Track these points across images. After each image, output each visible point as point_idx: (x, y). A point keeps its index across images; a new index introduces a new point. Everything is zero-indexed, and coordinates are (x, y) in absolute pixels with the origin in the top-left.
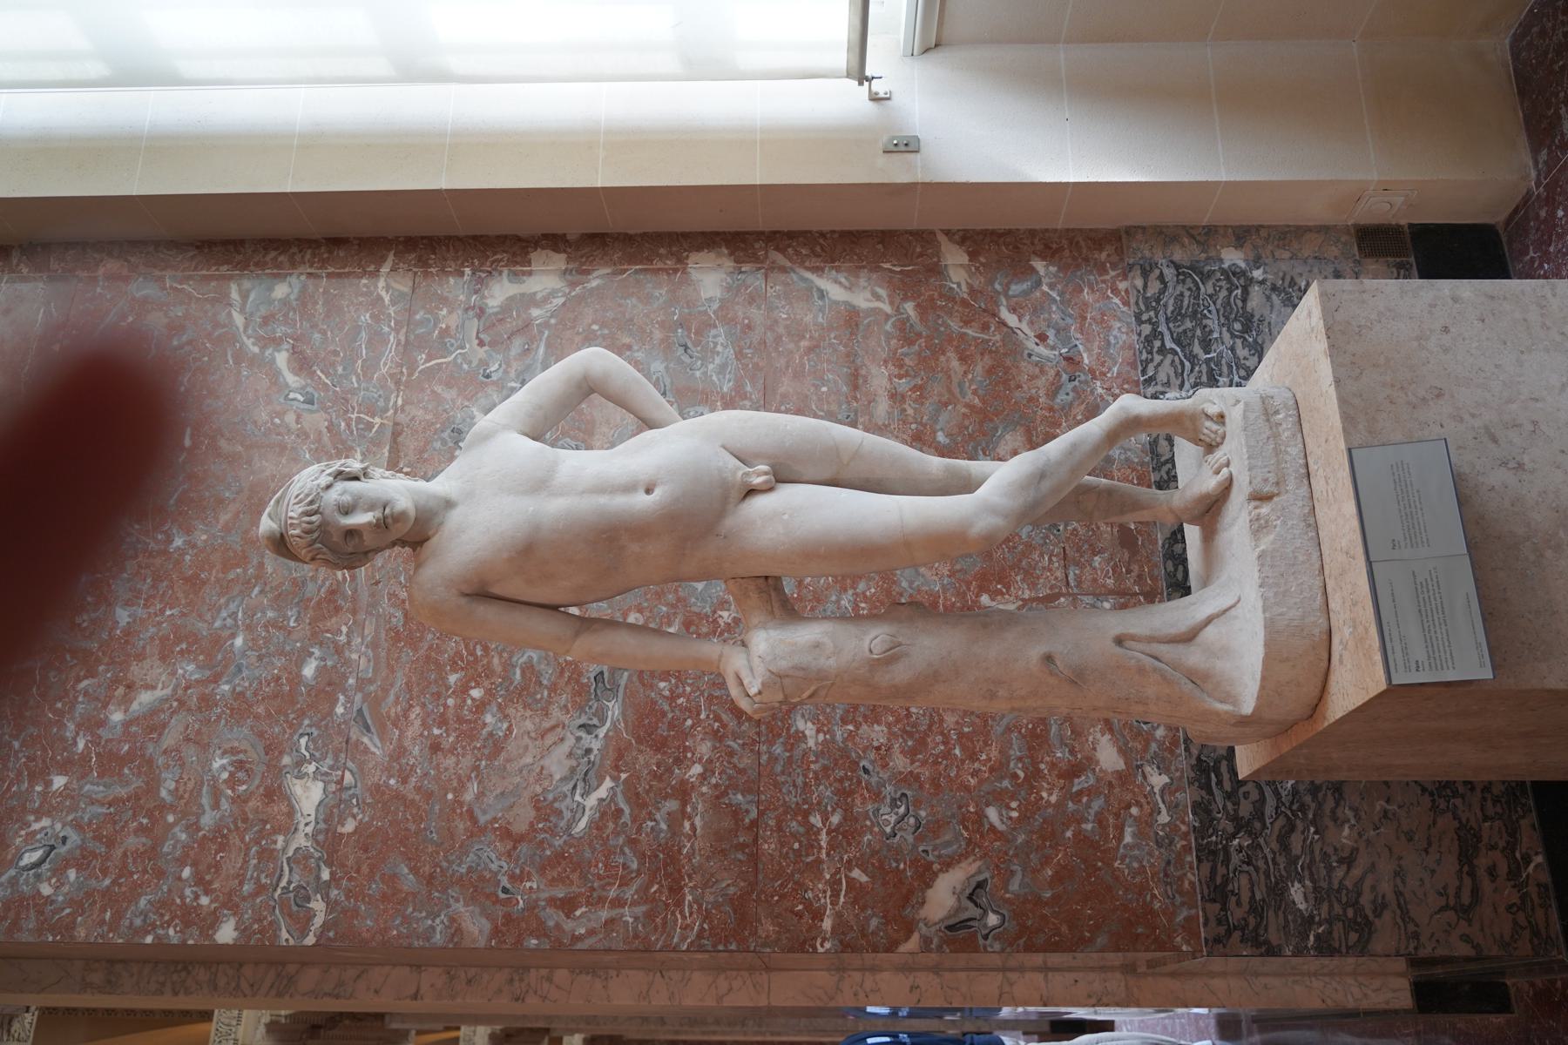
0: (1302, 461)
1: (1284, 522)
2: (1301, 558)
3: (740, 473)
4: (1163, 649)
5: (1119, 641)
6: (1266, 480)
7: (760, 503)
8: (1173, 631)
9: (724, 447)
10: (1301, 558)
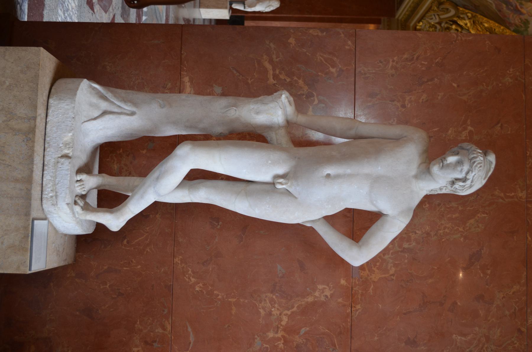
0: (45, 172)
2: (54, 128)
3: (289, 184)
4: (116, 110)
5: (133, 114)
6: (62, 164)
7: (281, 170)
8: (111, 116)
9: (296, 198)
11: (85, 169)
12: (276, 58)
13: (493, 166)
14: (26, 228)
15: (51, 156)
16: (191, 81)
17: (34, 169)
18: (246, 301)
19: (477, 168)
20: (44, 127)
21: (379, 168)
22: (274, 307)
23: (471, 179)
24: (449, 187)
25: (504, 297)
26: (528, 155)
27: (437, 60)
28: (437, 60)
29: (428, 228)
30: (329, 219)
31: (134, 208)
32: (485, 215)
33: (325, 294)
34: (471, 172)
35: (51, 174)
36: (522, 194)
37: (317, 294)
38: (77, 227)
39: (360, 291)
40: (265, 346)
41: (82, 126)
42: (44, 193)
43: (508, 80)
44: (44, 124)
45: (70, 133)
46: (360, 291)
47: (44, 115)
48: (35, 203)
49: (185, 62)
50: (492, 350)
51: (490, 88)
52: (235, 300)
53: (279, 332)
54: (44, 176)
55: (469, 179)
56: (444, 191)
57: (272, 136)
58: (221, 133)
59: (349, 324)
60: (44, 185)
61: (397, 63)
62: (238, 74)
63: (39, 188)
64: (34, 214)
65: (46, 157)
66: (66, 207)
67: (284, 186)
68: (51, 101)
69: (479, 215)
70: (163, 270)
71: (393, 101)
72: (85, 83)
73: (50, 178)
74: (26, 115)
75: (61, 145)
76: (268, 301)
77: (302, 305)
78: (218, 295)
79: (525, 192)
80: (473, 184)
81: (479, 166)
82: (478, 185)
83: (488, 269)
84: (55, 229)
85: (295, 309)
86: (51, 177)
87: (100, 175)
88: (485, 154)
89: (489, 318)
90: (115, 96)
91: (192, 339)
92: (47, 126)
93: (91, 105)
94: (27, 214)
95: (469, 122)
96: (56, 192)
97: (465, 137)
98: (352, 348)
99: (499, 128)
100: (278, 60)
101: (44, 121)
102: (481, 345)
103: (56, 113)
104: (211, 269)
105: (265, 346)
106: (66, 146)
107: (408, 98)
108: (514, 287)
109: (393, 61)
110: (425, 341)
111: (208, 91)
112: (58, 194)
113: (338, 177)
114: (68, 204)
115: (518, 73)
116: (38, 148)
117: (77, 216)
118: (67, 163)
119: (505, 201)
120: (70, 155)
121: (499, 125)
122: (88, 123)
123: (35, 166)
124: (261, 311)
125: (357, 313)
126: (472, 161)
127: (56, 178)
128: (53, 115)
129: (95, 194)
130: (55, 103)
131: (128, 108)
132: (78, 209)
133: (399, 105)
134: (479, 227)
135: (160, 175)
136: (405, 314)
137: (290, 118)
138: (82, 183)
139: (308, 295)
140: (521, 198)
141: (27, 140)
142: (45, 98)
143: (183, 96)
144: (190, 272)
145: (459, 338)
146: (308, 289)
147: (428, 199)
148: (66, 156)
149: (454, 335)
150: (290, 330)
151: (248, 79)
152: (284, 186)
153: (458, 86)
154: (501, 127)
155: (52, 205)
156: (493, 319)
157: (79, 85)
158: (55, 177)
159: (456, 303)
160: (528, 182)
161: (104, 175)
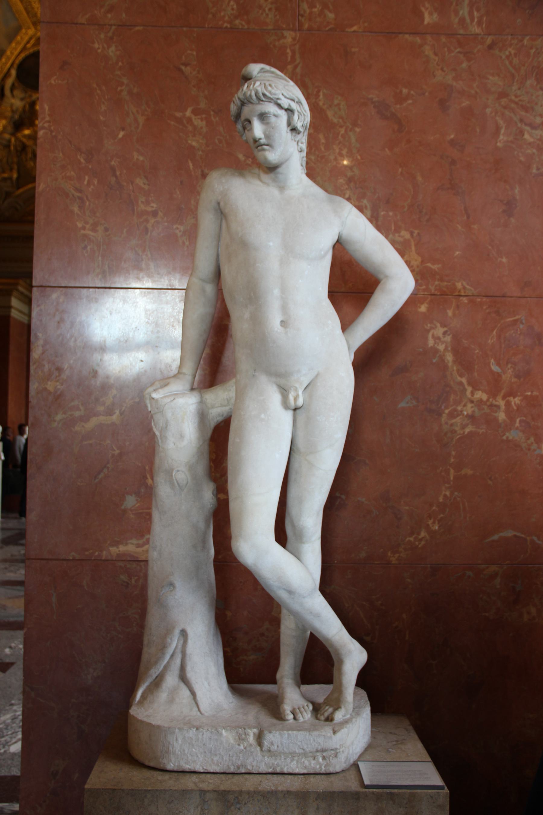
1: (241, 752)
2: (215, 759)
3: (297, 385)
4: (178, 661)
5: (184, 633)
6: (272, 744)
7: (275, 398)
8: (188, 668)
9: (317, 375)
10: (215, 759)
11: (273, 707)
12: (80, 410)
13: (267, 67)
14: (378, 798)
15: (260, 762)
16: (117, 544)
17: (285, 789)
18: (453, 453)
19: (273, 91)
20: (213, 776)
21: (271, 244)
22: (462, 411)
23: (290, 101)
24: (299, 137)
25: (442, 69)
26: (229, 26)
27: (82, 160)
28: (82, 160)
29: (341, 181)
30: (345, 326)
31: (330, 625)
32: (321, 94)
33: (441, 335)
34: (279, 101)
35: (288, 760)
36: (289, 37)
37: (441, 347)
38: (364, 715)
39: (437, 283)
40: (517, 424)
41: (206, 714)
42: (318, 771)
43: (112, 51)
44: (209, 776)
45: (221, 734)
46: (437, 283)
47: (194, 778)
48: (337, 785)
49: (87, 553)
50: (519, 89)
51: (125, 80)
52: (452, 471)
53: (497, 403)
54: (291, 771)
55: (290, 105)
56: (304, 146)
57: (216, 414)
58: (213, 494)
59: (484, 299)
60: (305, 771)
61: (87, 223)
62: (105, 470)
63: (312, 779)
64: (354, 786)
65: (261, 770)
66: (339, 735)
67: (300, 393)
68: (171, 766)
69: (321, 104)
70: (409, 580)
71: (146, 230)
72: (137, 712)
73: (295, 762)
74: (197, 807)
75: (242, 747)
76: (453, 421)
77: (458, 370)
78: (445, 496)
79: (286, 33)
80: (296, 100)
81: (270, 88)
82: (298, 93)
83: (401, 92)
84: (366, 750)
85: (464, 380)
86: (292, 760)
87: (279, 682)
88: (247, 78)
89: (473, 92)
90: (156, 663)
91: (509, 533)
92: (212, 771)
93: (171, 700)
94: (356, 796)
95: (179, 115)
96: (317, 751)
97: (202, 121)
98: (519, 295)
99: (188, 68)
100: (82, 408)
101: (203, 776)
102: (513, 105)
103: (190, 758)
104: (407, 508)
105: (517, 424)
106: (243, 740)
107: (142, 207)
108: (427, 53)
109: (84, 228)
110: (508, 187)
111: (132, 516)
112: (320, 748)
113: (284, 308)
114: (335, 732)
115: (102, 36)
116: (250, 783)
117: (348, 716)
118: (271, 736)
119: (299, 64)
120: (255, 730)
121: (183, 68)
122: (200, 704)
123: (280, 788)
124: (467, 430)
125: (468, 287)
126: (261, 98)
127: (295, 753)
128: (194, 762)
129: (305, 687)
130: (173, 760)
131: (174, 642)
132: (339, 716)
133: (152, 221)
134: (339, 105)
135: (285, 589)
136: (468, 217)
137: (188, 386)
138: (298, 711)
139: (443, 361)
140: (294, 39)
141: (238, 803)
142: (167, 776)
143: (154, 555)
144: (412, 539)
145: (501, 137)
146: (434, 361)
147: (311, 174)
148: (259, 738)
149: (499, 144)
150: (495, 386)
151: (113, 455)
152: (300, 393)
153: (123, 129)
154: (186, 65)
155: (336, 756)
156: (475, 85)
157: (142, 722)
158: (293, 755)
159: (452, 140)
160: (270, 27)
161: (278, 676)
